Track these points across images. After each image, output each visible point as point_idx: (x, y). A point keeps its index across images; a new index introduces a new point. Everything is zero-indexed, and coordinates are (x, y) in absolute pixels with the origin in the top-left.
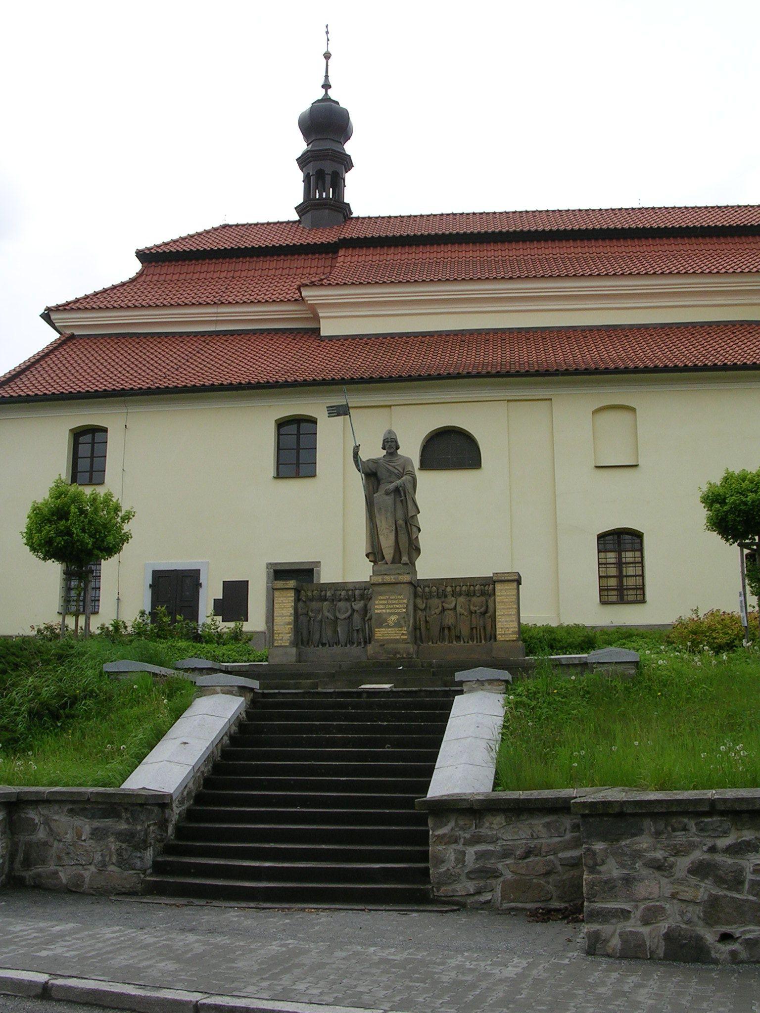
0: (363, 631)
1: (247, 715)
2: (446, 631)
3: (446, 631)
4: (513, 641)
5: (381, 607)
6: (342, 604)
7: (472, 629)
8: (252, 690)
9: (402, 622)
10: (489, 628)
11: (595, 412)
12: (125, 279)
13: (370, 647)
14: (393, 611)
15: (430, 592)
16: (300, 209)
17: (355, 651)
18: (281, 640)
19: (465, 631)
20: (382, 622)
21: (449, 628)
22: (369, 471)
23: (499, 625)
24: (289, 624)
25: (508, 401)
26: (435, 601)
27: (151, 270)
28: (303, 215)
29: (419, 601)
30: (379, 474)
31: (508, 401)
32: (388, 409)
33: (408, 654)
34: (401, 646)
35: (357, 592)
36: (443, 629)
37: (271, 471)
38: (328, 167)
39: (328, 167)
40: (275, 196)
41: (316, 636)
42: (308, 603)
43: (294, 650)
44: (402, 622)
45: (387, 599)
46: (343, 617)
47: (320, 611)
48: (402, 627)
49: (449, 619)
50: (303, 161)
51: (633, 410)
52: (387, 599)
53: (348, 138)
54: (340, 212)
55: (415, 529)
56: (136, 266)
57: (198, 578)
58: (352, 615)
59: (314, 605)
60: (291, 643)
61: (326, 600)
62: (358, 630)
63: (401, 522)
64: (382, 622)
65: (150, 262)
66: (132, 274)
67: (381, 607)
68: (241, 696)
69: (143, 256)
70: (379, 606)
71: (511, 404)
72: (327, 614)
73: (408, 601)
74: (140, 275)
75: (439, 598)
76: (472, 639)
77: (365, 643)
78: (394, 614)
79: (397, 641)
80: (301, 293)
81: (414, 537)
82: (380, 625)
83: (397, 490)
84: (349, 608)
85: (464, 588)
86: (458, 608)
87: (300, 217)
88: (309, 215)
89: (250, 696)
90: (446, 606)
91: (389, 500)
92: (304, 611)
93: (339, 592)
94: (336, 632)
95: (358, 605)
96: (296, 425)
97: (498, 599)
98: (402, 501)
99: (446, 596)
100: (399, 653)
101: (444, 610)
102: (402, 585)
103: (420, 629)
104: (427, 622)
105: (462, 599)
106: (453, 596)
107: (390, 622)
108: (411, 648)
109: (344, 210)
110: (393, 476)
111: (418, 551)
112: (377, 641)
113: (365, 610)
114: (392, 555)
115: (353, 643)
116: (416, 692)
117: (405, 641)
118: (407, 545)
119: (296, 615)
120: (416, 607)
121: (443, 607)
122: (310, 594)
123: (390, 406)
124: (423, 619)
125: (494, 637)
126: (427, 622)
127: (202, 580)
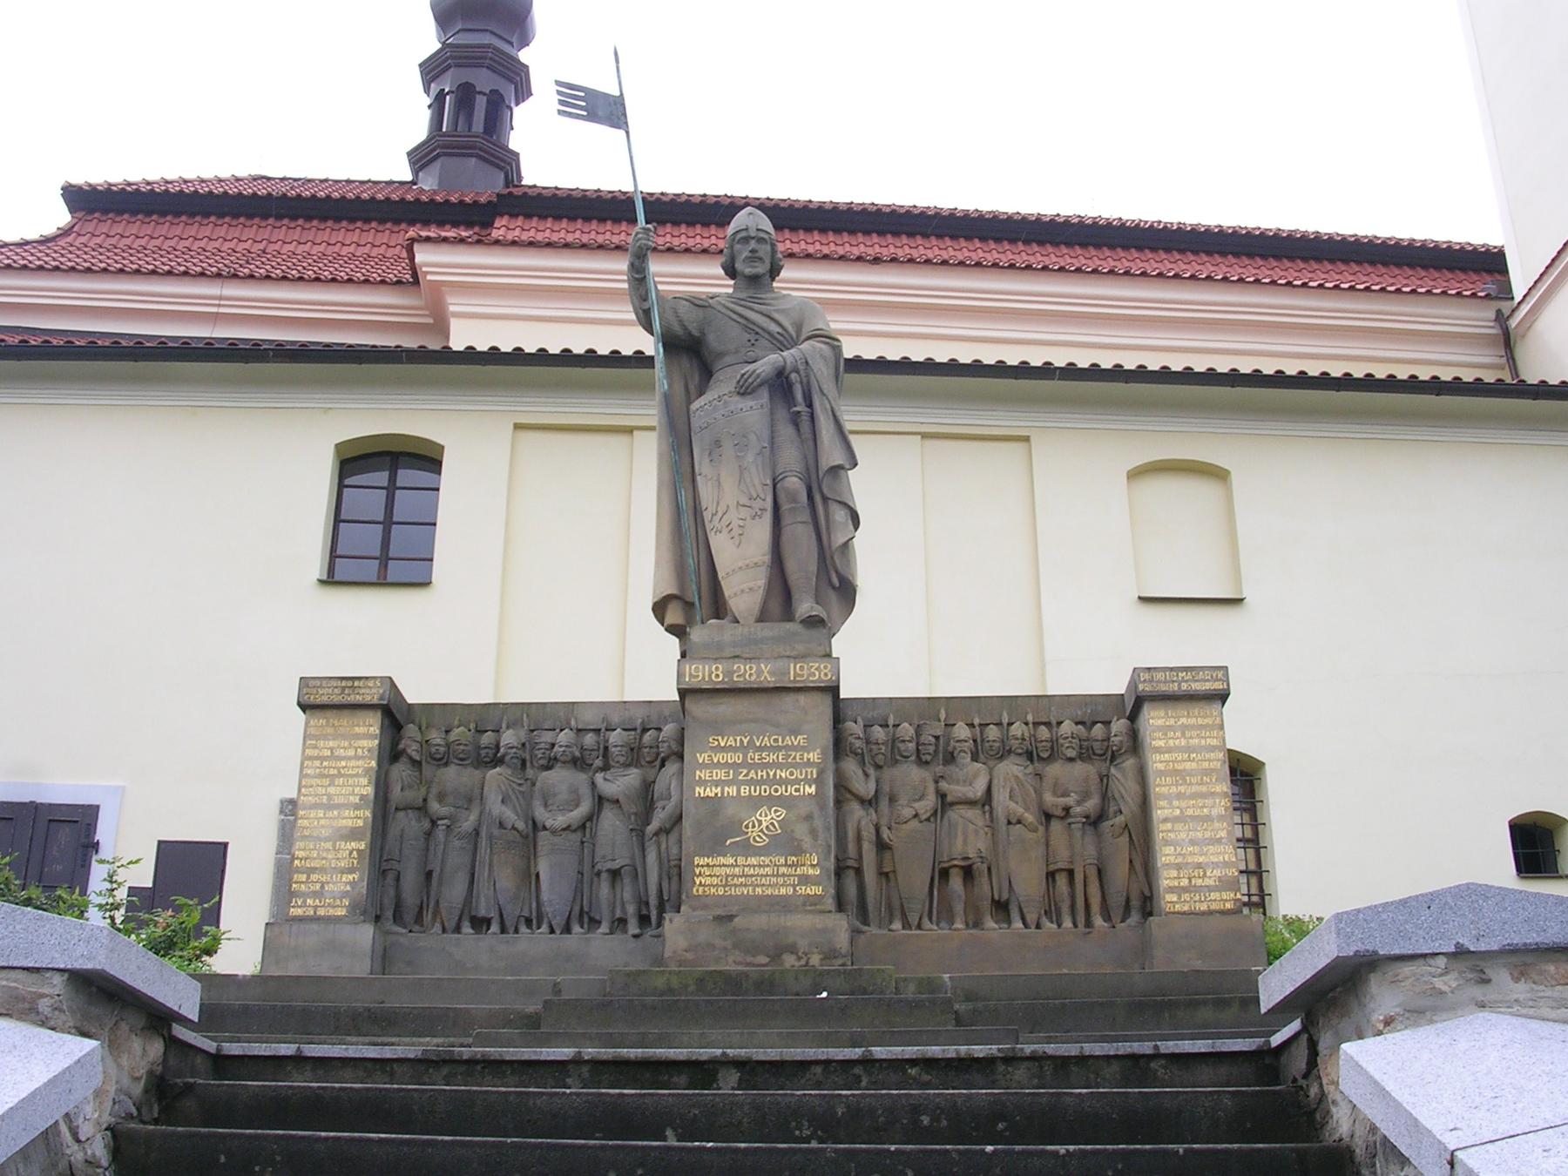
0: (638, 873)
1: (116, 1152)
2: (956, 882)
3: (956, 882)
4: (1223, 912)
5: (720, 774)
6: (560, 779)
7: (1051, 875)
8: (158, 1019)
9: (801, 831)
10: (1119, 872)
11: (1136, 474)
12: (33, 235)
13: (674, 925)
14: (765, 790)
15: (894, 741)
16: (420, 158)
17: (604, 952)
18: (315, 895)
19: (1027, 881)
20: (722, 833)
21: (968, 873)
22: (677, 329)
23: (1165, 856)
24: (353, 834)
25: (925, 436)
26: (911, 774)
27: (90, 227)
28: (422, 168)
29: (851, 766)
30: (712, 339)
31: (925, 436)
32: (622, 440)
33: (830, 954)
34: (801, 922)
35: (615, 737)
36: (945, 874)
37: (314, 561)
38: (484, 80)
39: (484, 80)
40: (374, 134)
41: (453, 893)
42: (428, 770)
43: (365, 934)
44: (801, 831)
45: (744, 749)
46: (560, 820)
47: (473, 798)
48: (798, 850)
49: (968, 837)
50: (431, 70)
51: (1218, 474)
52: (744, 749)
53: (525, 42)
54: (501, 168)
55: (840, 515)
56: (59, 216)
57: (91, 827)
58: (591, 817)
59: (454, 776)
60: (353, 908)
61: (497, 761)
62: (615, 874)
63: (794, 483)
64: (722, 833)
65: (91, 211)
66: (50, 230)
67: (720, 774)
68: (85, 1034)
69: (77, 197)
70: (713, 773)
71: (929, 443)
72: (495, 807)
73: (824, 760)
74: (65, 232)
75: (921, 762)
76: (1052, 912)
77: (644, 920)
78: (771, 801)
79: (783, 905)
80: (412, 258)
81: (839, 539)
82: (715, 846)
83: (781, 385)
84: (585, 790)
85: (1018, 729)
86: (1001, 798)
87: (416, 172)
88: (436, 167)
89: (146, 1053)
90: (954, 790)
91: (754, 412)
92: (414, 796)
93: (547, 737)
94: (530, 878)
95: (621, 783)
96: (378, 554)
97: (1156, 763)
98: (795, 420)
99: (950, 758)
100: (792, 949)
101: (945, 803)
102: (802, 699)
103: (859, 871)
104: (882, 846)
105: (1011, 768)
106: (975, 758)
107: (753, 833)
108: (839, 927)
109: (508, 163)
110: (764, 342)
111: (846, 592)
112: (703, 903)
113: (647, 796)
114: (758, 597)
115: (595, 923)
116: (989, 1062)
117: (811, 902)
118: (813, 567)
119: (383, 806)
120: (843, 790)
121: (942, 796)
122: (436, 737)
123: (629, 431)
124: (868, 834)
125: (1147, 904)
126: (882, 846)
127: (103, 834)
